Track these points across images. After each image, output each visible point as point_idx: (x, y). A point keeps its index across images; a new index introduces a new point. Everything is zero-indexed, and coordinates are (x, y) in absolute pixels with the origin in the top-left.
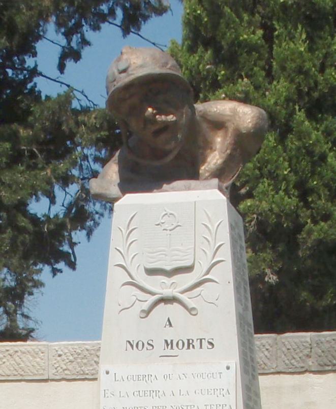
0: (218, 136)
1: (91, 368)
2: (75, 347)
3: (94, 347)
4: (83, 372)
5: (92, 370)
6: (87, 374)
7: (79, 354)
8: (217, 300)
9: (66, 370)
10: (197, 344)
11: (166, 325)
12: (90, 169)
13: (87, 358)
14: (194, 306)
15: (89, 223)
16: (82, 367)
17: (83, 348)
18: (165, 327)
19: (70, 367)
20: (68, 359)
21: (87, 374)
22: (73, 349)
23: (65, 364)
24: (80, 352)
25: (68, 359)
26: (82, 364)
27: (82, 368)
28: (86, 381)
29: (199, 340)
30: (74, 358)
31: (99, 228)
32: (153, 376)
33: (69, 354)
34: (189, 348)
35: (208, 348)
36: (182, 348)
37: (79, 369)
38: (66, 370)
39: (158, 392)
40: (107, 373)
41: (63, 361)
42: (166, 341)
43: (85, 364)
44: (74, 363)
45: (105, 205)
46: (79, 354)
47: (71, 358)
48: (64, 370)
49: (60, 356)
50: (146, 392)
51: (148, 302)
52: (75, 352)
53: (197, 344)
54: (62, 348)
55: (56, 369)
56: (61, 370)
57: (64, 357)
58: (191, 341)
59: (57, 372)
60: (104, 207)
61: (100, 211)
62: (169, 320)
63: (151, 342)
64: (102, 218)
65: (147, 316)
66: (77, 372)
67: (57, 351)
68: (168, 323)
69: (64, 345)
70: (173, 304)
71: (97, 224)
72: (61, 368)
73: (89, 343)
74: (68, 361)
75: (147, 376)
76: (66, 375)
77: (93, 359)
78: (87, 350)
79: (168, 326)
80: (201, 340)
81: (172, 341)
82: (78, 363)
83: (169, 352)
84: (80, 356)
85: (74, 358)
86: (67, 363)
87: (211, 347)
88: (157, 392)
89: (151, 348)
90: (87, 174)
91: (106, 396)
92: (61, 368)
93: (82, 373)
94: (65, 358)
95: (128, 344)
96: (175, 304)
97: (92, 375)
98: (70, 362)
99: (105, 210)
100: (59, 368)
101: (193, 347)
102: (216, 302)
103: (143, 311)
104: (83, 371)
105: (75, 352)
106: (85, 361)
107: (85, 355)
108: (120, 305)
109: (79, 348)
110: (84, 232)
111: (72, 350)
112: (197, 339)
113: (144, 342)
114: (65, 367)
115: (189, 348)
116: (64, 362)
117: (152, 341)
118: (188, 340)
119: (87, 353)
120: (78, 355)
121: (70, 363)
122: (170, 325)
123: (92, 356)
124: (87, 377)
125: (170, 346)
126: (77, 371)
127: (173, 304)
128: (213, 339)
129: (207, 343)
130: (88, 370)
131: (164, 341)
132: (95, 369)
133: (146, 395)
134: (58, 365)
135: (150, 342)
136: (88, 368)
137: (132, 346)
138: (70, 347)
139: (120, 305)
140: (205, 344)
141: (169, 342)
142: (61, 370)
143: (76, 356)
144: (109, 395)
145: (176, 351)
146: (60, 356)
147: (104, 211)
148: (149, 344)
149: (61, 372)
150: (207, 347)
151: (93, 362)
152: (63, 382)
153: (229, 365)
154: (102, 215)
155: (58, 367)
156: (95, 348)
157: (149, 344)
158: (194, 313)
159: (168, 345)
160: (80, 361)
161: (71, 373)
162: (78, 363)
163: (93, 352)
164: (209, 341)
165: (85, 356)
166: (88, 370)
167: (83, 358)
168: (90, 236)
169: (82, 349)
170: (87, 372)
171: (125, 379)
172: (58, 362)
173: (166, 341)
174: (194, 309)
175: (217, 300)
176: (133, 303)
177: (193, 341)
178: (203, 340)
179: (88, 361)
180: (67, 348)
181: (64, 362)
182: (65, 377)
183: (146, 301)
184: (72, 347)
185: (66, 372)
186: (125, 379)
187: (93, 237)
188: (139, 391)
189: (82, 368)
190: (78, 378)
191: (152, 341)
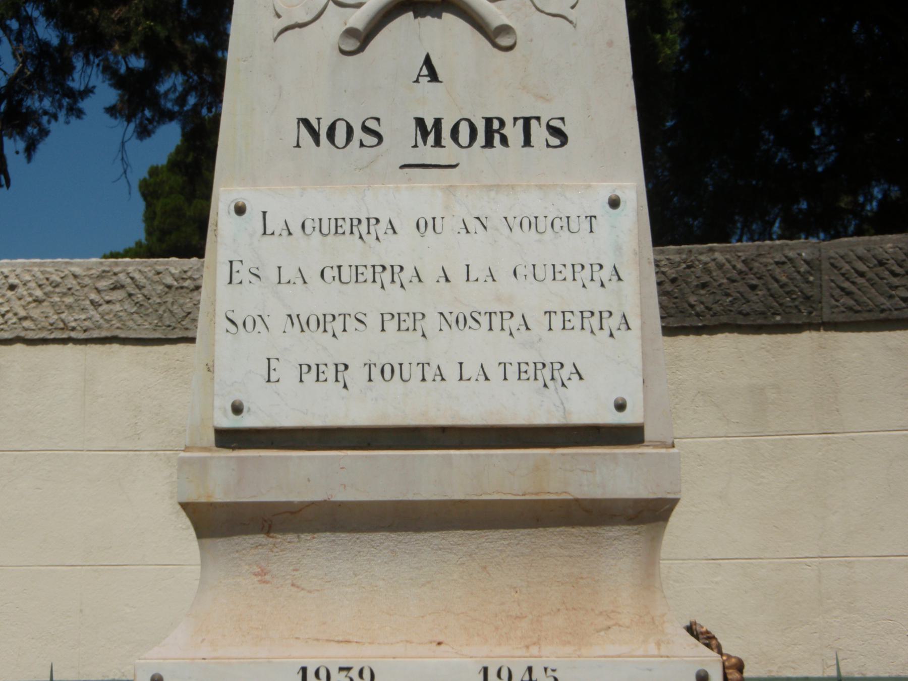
0: (191, 96)
1: (83, 317)
2: (48, 269)
3: (90, 269)
4: (65, 324)
5: (85, 320)
6: (73, 329)
7: (57, 286)
8: (573, 7)
9: (25, 318)
10: (514, 133)
11: (419, 75)
12: (35, 39)
13: (73, 294)
14: (504, 20)
15: (32, 130)
16: (63, 312)
17: (67, 272)
18: (417, 81)
19: (35, 313)
20: (31, 295)
21: (73, 329)
22: (43, 272)
23: (24, 307)
24: (59, 280)
25: (31, 295)
26: (63, 307)
27: (63, 316)
28: (70, 345)
29: (520, 123)
30: (45, 294)
31: (48, 140)
32: (384, 224)
33: (33, 285)
34: (489, 143)
35: (548, 146)
36: (471, 144)
37: (55, 317)
38: (25, 318)
39: (396, 270)
40: (240, 210)
41: (20, 299)
42: (420, 122)
43: (69, 307)
44: (45, 304)
45: (60, 101)
46: (57, 286)
47: (39, 293)
48: (20, 319)
49: (12, 287)
50: (361, 270)
51: (363, 8)
52: (47, 279)
53: (514, 133)
54: (18, 271)
55: (3, 316)
56: (14, 320)
57: (21, 291)
58: (496, 125)
59: (6, 322)
60: (57, 104)
61: (52, 110)
62: (428, 62)
63: (375, 122)
64: (53, 122)
65: (361, 49)
66: (51, 325)
67: (6, 277)
68: (425, 71)
69: (24, 264)
70: (440, 17)
71: (44, 133)
72: (16, 314)
73: (80, 263)
74: (30, 299)
75: (365, 222)
76: (25, 329)
77: (87, 297)
78: (75, 276)
79: (424, 80)
80: (527, 121)
81: (438, 122)
82: (53, 304)
83: (428, 153)
84: (57, 290)
85: (45, 294)
86: (29, 303)
87: (555, 141)
88: (397, 269)
89: (375, 140)
90: (30, 46)
91: (235, 281)
92: (16, 314)
93: (61, 325)
94: (25, 293)
95: (303, 130)
96: (448, 17)
97: (85, 331)
98: (35, 301)
99: (60, 110)
100: (10, 315)
101: (504, 141)
102: (572, 14)
103: (350, 33)
104: (63, 321)
105: (47, 279)
106: (69, 300)
107: (69, 286)
108: (279, 16)
109: (56, 270)
110: (21, 145)
111: (41, 277)
112: (516, 119)
113: (352, 124)
114: (22, 313)
115: (489, 143)
116: (23, 302)
117: (378, 120)
118: (489, 121)
119: (74, 282)
120: (55, 287)
121: (34, 305)
122: (433, 76)
123: (86, 289)
124: (73, 335)
125: (431, 138)
126: (51, 321)
127: (440, 17)
128: (562, 119)
129: (545, 134)
130: (76, 320)
131: (413, 123)
132: (90, 319)
133: (361, 278)
134: (8, 309)
135: (372, 124)
136: (77, 317)
137: (315, 135)
138: (36, 269)
139: (279, 16)
140: (539, 133)
141: (429, 124)
142: (14, 320)
143: (50, 288)
144: (245, 275)
145: (449, 152)
146: (12, 287)
147: (58, 110)
148: (366, 129)
149: (15, 324)
150: (564, 122)
151: (88, 302)
152: (19, 347)
153: (619, 193)
154: (55, 117)
155: (7, 312)
156: (93, 272)
157: (366, 129)
158: (504, 41)
159: (425, 134)
160: (58, 299)
161: (36, 325)
162: (53, 304)
163: (87, 281)
164: (552, 123)
165: (70, 289)
166: (76, 320)
167: (64, 294)
168: (33, 153)
169: (62, 275)
170: (73, 324)
171: (296, 228)
172: (8, 301)
173: (420, 122)
174: (505, 29)
175: (573, 7)
176: (319, 9)
177: (502, 123)
178: (534, 123)
179: (76, 301)
180: (28, 271)
181: (23, 302)
182: (23, 334)
183: (358, 6)
184: (42, 269)
185: (27, 324)
186: (296, 228)
187: (38, 155)
188: (339, 267)
189: (63, 316)
190: (52, 336)
191: (378, 120)
